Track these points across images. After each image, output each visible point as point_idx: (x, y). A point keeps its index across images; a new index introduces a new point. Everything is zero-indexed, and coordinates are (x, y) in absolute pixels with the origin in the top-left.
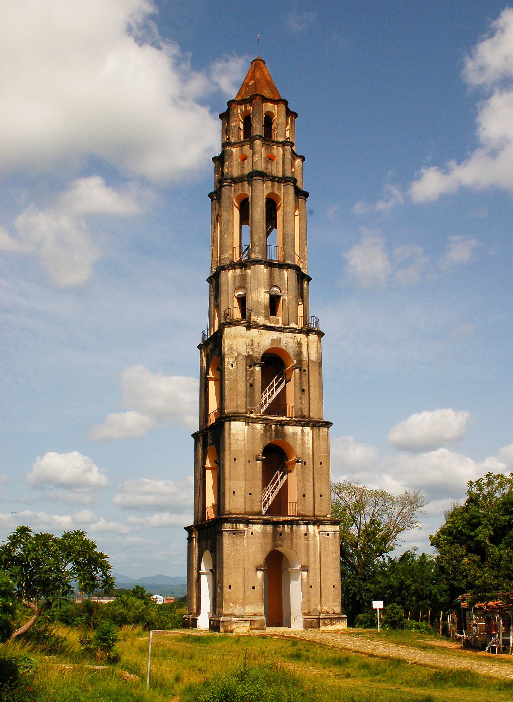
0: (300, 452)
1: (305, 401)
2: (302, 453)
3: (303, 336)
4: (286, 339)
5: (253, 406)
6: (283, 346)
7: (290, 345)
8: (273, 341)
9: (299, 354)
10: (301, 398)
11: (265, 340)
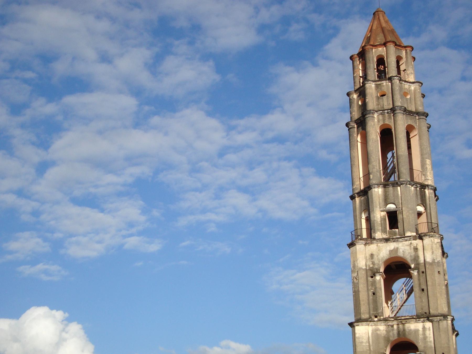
0: (423, 346)
1: (425, 300)
2: (424, 347)
3: (418, 242)
4: (403, 248)
5: (377, 311)
6: (400, 254)
7: (407, 252)
8: (391, 251)
9: (416, 258)
10: (420, 298)
11: (383, 251)
